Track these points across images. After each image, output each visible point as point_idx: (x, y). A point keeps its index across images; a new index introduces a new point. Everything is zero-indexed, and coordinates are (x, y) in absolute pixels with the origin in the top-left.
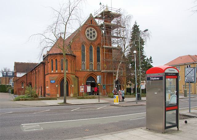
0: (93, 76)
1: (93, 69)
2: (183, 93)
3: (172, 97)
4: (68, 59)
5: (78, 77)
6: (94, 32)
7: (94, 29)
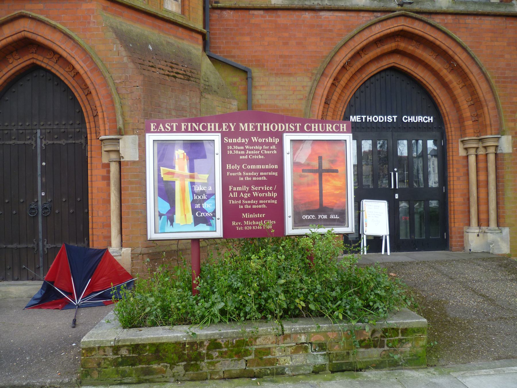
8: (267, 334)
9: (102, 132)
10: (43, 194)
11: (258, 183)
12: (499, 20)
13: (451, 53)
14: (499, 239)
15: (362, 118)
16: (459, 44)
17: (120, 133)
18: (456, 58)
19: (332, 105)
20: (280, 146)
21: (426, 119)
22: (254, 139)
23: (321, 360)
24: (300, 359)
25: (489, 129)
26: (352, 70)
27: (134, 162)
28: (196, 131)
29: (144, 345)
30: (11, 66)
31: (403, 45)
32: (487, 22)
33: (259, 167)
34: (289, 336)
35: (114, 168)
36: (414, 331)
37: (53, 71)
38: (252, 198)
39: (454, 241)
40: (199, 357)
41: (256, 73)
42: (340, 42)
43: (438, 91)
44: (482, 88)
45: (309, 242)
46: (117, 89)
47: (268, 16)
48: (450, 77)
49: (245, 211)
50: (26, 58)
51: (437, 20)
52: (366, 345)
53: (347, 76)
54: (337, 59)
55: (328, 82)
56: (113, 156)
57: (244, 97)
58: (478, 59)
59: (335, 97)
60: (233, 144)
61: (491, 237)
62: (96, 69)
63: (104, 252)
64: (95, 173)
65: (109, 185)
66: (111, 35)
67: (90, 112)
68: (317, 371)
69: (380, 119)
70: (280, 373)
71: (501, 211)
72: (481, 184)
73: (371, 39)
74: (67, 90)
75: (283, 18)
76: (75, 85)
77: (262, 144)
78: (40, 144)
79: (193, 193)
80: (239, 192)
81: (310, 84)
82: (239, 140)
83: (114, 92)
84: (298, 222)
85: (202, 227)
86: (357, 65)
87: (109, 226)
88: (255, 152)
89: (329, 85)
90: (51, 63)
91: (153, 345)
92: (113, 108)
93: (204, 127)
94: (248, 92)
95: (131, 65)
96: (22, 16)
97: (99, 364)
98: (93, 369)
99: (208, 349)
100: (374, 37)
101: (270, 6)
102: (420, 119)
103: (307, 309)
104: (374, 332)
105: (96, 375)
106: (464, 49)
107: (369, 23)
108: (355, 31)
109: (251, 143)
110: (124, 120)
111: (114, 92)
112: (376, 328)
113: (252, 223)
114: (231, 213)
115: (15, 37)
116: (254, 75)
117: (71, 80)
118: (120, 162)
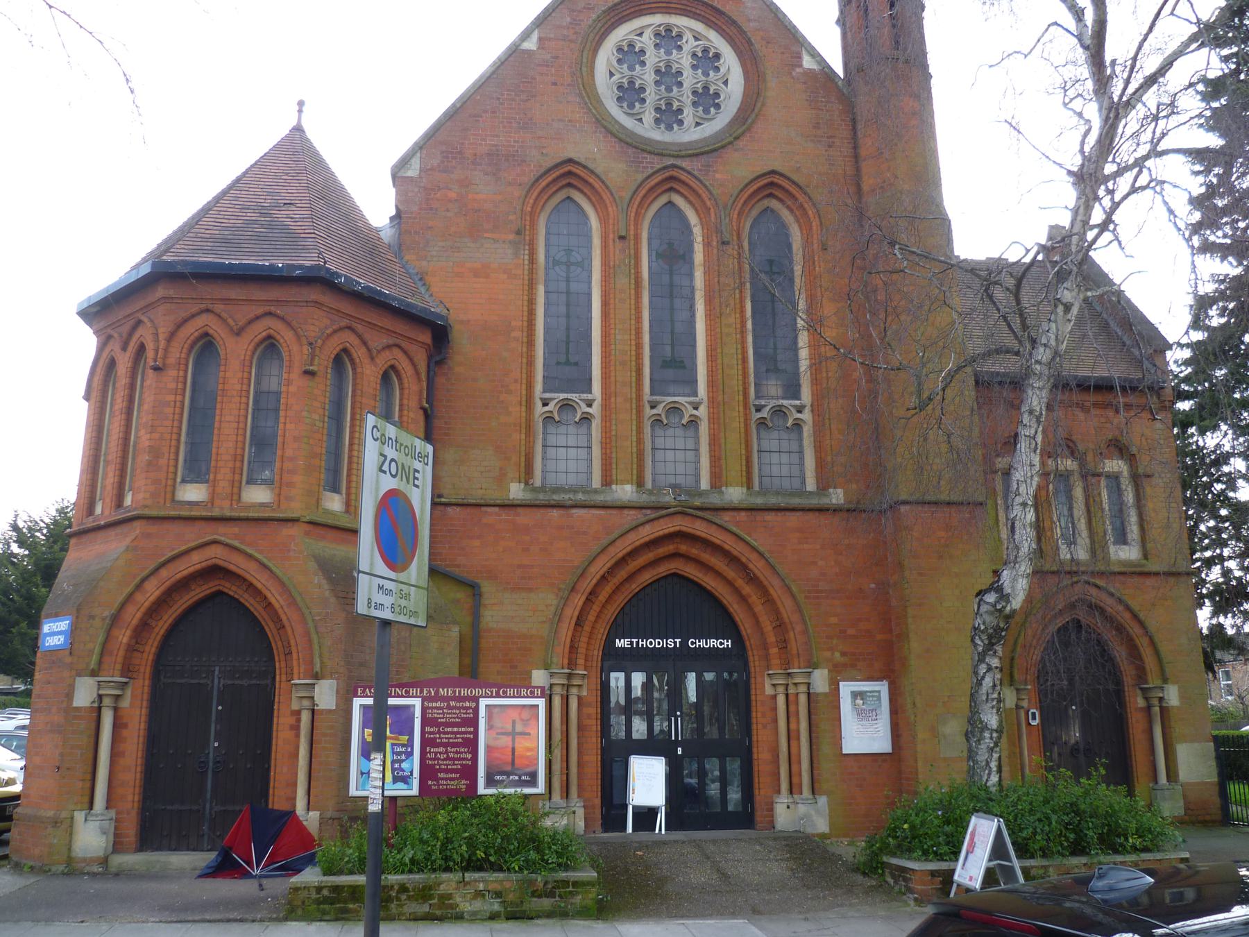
1: (705, 484)
5: (474, 589)
6: (707, 60)
8: (449, 880)
9: (295, 675)
10: (216, 744)
11: (454, 745)
12: (810, 515)
13: (744, 560)
14: (813, 813)
15: (632, 643)
16: (754, 549)
17: (317, 677)
18: (751, 566)
19: (587, 628)
20: (476, 710)
21: (721, 644)
22: (453, 704)
24: (478, 905)
25: (796, 660)
26: (616, 580)
27: (330, 711)
28: (399, 696)
29: (343, 887)
30: (193, 593)
31: (683, 548)
32: (793, 519)
33: (455, 729)
34: (468, 883)
35: (305, 717)
37: (242, 600)
38: (448, 758)
39: (759, 815)
40: (389, 899)
41: (487, 588)
42: (596, 548)
43: (736, 606)
44: (786, 607)
45: (492, 801)
46: (316, 627)
47: (505, 515)
48: (747, 589)
49: (441, 771)
50: (211, 585)
51: (726, 518)
52: (534, 894)
53: (650, 556)
54: (593, 569)
55: (579, 600)
56: (306, 703)
57: (469, 619)
58: (779, 568)
59: (591, 617)
60: (432, 708)
61: (802, 809)
62: (293, 603)
63: (291, 814)
64: (282, 722)
65: (298, 736)
66: (312, 565)
67: (281, 650)
68: (493, 917)
69: (657, 643)
70: (459, 917)
71: (815, 772)
72: (792, 735)
73: (638, 543)
75: (524, 518)
76: (266, 617)
77: (459, 708)
78: (217, 683)
79: (393, 753)
80: (436, 753)
81: (555, 602)
82: (438, 704)
83: (312, 630)
84: (490, 782)
85: (400, 785)
86: (623, 574)
87: (295, 785)
88: (452, 716)
89: (581, 603)
90: (240, 592)
91: (350, 886)
92: (311, 648)
93: (407, 692)
95: (333, 600)
96: (215, 542)
97: (303, 903)
98: (298, 907)
99: (398, 892)
100: (642, 541)
101: (507, 502)
102: (713, 643)
103: (486, 860)
104: (546, 883)
105: (300, 912)
106: (761, 555)
107: (634, 523)
108: (615, 535)
109: (449, 707)
110: (322, 663)
111: (312, 630)
112: (550, 879)
114: (427, 772)
115: (204, 564)
116: (484, 590)
117: (262, 611)
118: (313, 711)
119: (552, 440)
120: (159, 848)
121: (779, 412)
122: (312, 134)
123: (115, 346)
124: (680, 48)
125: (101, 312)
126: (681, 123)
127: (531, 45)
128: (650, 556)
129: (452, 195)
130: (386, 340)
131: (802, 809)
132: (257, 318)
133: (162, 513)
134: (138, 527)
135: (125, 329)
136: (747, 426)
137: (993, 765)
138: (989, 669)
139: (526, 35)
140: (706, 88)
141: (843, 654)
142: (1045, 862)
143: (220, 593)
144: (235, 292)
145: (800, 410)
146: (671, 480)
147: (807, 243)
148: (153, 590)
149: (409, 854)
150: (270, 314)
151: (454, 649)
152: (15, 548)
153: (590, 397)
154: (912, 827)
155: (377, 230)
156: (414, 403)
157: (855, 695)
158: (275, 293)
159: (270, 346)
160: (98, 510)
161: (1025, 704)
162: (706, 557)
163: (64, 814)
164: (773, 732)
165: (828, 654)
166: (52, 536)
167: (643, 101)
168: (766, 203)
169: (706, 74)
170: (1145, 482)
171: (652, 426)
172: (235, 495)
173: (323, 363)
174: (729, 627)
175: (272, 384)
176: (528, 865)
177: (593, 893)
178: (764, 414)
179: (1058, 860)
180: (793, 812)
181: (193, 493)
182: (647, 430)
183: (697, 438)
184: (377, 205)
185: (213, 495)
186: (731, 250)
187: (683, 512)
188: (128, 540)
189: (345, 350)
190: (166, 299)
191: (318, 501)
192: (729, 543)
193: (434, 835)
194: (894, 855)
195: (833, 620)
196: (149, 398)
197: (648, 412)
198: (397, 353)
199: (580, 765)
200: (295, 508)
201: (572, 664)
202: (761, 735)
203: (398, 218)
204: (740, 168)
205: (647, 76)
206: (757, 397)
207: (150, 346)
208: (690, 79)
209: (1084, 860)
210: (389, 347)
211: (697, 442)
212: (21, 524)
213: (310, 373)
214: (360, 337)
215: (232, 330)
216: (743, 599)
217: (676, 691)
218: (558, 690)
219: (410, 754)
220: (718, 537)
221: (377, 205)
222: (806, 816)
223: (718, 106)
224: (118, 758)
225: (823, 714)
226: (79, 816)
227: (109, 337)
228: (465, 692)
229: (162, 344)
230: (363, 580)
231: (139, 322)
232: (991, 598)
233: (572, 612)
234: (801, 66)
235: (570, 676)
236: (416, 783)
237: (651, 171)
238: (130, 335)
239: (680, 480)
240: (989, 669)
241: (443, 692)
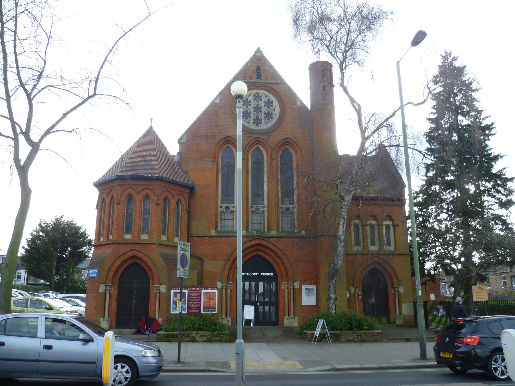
0: (266, 253)
1: (266, 230)
2: (83, 307)
3: (342, 85)
4: (152, 194)
5: (201, 260)
6: (269, 103)
7: (266, 93)
16: (279, 248)
17: (161, 284)
23: (205, 339)
24: (201, 339)
31: (259, 248)
35: (158, 294)
36: (226, 334)
41: (205, 259)
44: (287, 264)
48: (277, 260)
51: (271, 240)
52: (214, 336)
53: (250, 250)
56: (158, 291)
62: (154, 265)
63: (155, 318)
64: (152, 296)
65: (156, 299)
68: (204, 341)
69: (252, 274)
70: (196, 341)
74: (144, 270)
75: (215, 240)
84: (204, 311)
88: (195, 294)
94: (202, 266)
95: (165, 264)
96: (134, 250)
102: (268, 274)
106: (280, 250)
113: (194, 310)
114: (189, 308)
119: (223, 217)
120: (121, 328)
121: (288, 209)
122: (155, 129)
123: (105, 196)
124: (261, 100)
125: (100, 185)
126: (261, 123)
127: (217, 101)
128: (250, 250)
129: (195, 147)
130: (177, 193)
131: (291, 320)
132: (144, 189)
133: (121, 242)
134: (114, 246)
135: (108, 191)
136: (278, 213)
137: (334, 308)
138: (332, 283)
139: (216, 98)
140: (269, 112)
141: (303, 278)
142: (341, 332)
143: (135, 262)
144: (138, 183)
145: (294, 208)
146: (256, 229)
147: (297, 160)
148: (119, 262)
149: (185, 327)
150: (147, 188)
151: (196, 276)
152: (41, 233)
153: (233, 205)
154: (310, 323)
155: (173, 156)
156: (185, 209)
157: (306, 289)
158: (148, 183)
159: (147, 197)
160: (102, 239)
161: (358, 292)
162: (266, 250)
163: (98, 319)
164: (284, 300)
165: (299, 278)
166: (53, 229)
167: (250, 117)
168: (285, 146)
169: (269, 108)
170: (396, 227)
171: (251, 213)
172: (139, 237)
173: (161, 201)
174: (272, 270)
175: (147, 206)
176: (213, 330)
177: (228, 337)
178: (283, 209)
179: (344, 332)
180: (291, 321)
181: (128, 236)
182: (250, 214)
183: (264, 217)
184: (173, 149)
185: (133, 237)
186: (274, 162)
187: (259, 238)
188: (111, 249)
189: (166, 197)
190: (119, 185)
191: (160, 238)
192: (272, 247)
193: (191, 323)
194: (305, 330)
195: (301, 268)
196: (116, 212)
197: (250, 209)
198: (180, 196)
199: (230, 307)
200: (155, 240)
201: (228, 280)
202: (281, 300)
203: (179, 153)
204: (278, 137)
205: (251, 109)
206: (282, 205)
207: (115, 197)
208: (264, 110)
209: (352, 332)
210: (178, 195)
211: (264, 218)
212: (43, 225)
213: (158, 204)
214: (170, 193)
215: (137, 192)
216: (276, 262)
217: (257, 287)
218: (224, 287)
219: (185, 304)
220: (269, 245)
221: (173, 149)
222: (292, 322)
223: (272, 118)
224: (110, 305)
225: (297, 294)
226: (102, 319)
227: (103, 192)
228: (198, 289)
229: (119, 197)
230: (178, 271)
231: (112, 190)
232: (332, 265)
233: (228, 266)
234: (296, 105)
235: (227, 284)
236: (186, 310)
237: (251, 139)
238: (109, 193)
239: (259, 229)
240: (332, 283)
241: (193, 289)
